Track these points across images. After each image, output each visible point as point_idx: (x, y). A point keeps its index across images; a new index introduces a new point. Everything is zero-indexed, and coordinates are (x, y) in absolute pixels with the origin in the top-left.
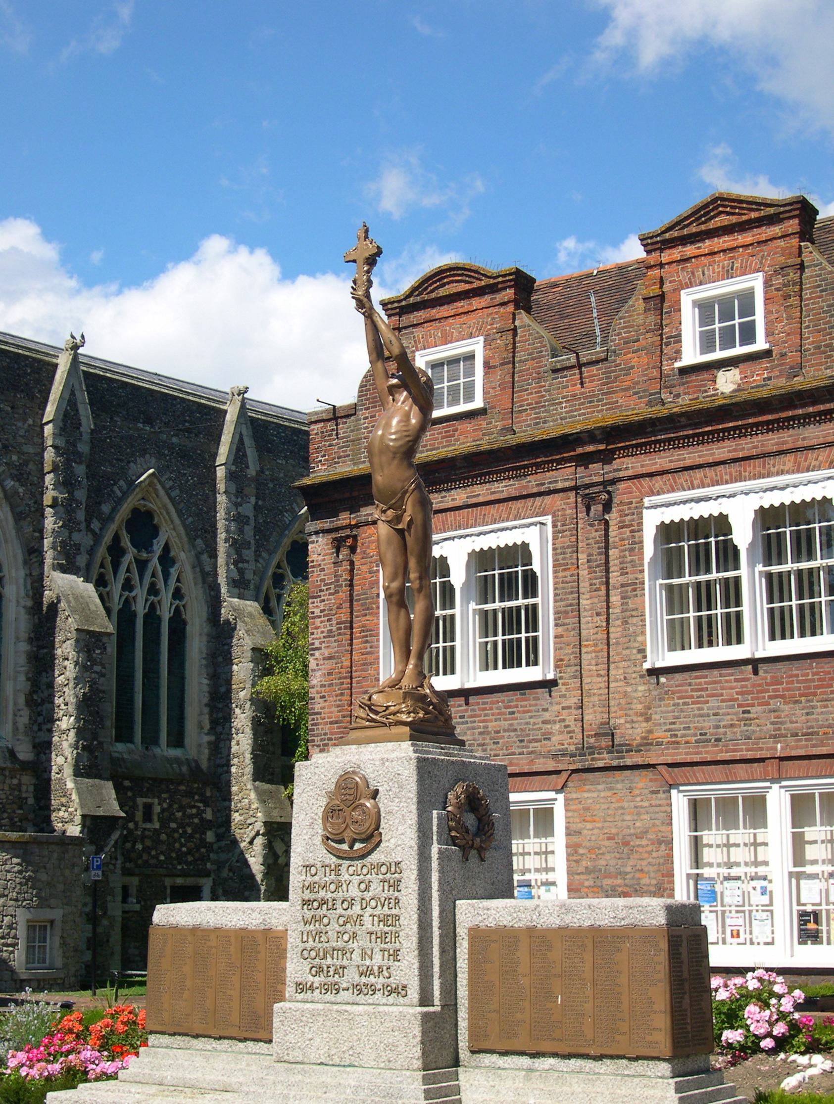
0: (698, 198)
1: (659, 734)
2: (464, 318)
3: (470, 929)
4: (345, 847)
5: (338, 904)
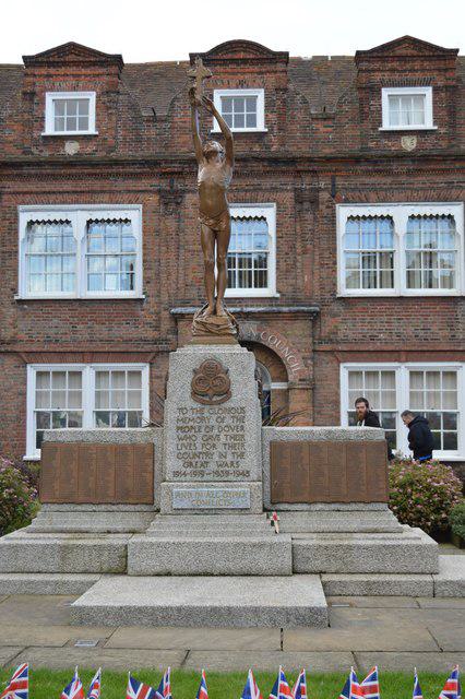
1: (22, 335)
3: (271, 442)
5: (203, 430)
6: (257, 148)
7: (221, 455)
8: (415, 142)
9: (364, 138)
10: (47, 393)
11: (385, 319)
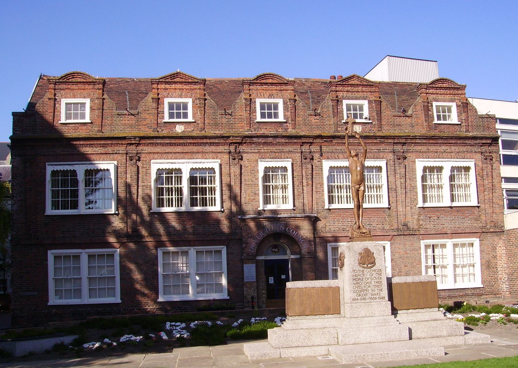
0: (173, 71)
2: (82, 91)
4: (365, 266)
6: (280, 130)
7: (372, 290)
8: (361, 128)
9: (337, 125)
10: (95, 267)
11: (349, 220)
